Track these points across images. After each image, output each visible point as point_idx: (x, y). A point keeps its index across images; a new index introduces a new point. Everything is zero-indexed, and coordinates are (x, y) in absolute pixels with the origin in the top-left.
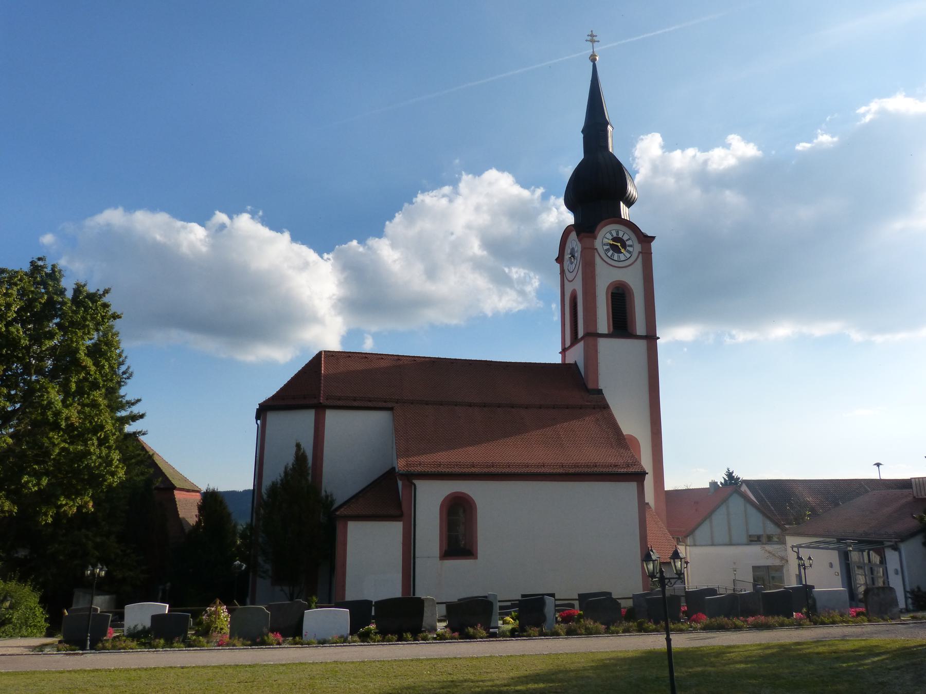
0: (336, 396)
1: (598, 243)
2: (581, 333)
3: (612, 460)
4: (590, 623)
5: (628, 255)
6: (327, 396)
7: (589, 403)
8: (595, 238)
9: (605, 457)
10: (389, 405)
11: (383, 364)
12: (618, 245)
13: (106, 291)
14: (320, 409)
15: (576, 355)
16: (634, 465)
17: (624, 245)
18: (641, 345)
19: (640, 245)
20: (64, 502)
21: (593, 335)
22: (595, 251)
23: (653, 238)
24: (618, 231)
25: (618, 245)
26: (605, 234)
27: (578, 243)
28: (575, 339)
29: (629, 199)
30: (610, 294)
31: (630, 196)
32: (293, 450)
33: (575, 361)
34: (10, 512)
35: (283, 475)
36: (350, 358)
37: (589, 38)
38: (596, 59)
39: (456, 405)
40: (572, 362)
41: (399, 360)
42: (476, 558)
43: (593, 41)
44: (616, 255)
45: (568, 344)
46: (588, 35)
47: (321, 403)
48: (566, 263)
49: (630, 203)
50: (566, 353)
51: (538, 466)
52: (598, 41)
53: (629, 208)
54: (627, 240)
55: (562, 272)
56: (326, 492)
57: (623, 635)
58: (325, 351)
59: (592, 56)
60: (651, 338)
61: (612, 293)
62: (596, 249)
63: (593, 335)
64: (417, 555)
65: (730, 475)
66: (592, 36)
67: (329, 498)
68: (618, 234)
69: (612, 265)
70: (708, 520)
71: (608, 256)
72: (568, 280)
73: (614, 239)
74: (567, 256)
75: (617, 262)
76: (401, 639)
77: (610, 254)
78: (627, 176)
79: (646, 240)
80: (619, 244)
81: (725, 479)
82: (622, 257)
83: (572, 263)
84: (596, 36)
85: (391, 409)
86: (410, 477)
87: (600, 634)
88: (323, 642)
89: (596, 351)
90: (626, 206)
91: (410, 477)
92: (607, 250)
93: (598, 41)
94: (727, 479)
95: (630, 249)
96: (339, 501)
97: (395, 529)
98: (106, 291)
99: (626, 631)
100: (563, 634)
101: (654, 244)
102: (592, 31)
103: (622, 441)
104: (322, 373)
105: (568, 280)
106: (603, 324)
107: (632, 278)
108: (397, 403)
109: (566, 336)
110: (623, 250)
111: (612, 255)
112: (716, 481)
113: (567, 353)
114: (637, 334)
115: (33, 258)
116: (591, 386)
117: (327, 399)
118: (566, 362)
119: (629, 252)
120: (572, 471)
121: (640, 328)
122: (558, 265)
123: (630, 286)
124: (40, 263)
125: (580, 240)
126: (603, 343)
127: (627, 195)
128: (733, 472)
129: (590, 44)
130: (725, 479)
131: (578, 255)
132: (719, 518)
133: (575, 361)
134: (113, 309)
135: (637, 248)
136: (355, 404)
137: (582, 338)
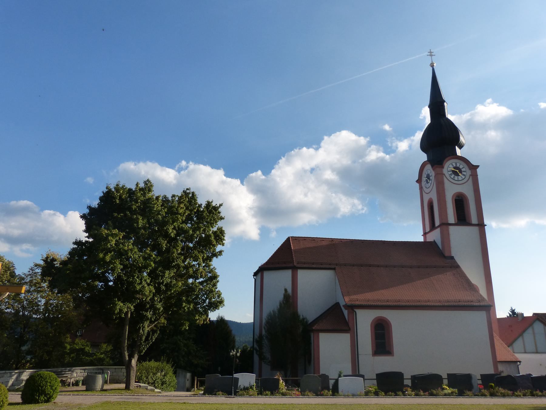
0: (302, 262)
1: (445, 171)
2: (437, 223)
3: (469, 298)
4: (502, 390)
5: (464, 177)
6: (298, 262)
7: (447, 265)
8: (443, 167)
9: (463, 296)
10: (333, 267)
11: (324, 243)
12: (456, 172)
13: (221, 205)
14: (294, 269)
15: (435, 236)
16: (483, 301)
17: (461, 171)
18: (476, 229)
19: (470, 171)
20: (197, 318)
21: (445, 224)
22: (444, 175)
23: (478, 166)
24: (456, 163)
25: (456, 172)
26: (449, 165)
27: (432, 171)
28: (433, 227)
29: (460, 144)
30: (454, 200)
31: (462, 142)
32: (283, 292)
33: (434, 240)
34: (164, 323)
35: (279, 307)
36: (305, 241)
37: (429, 54)
38: (434, 66)
39: (370, 266)
40: (432, 240)
41: (332, 241)
42: (393, 355)
43: (431, 55)
44: (456, 177)
45: (428, 229)
46: (428, 52)
47: (295, 266)
48: (424, 183)
49: (461, 147)
50: (427, 235)
51: (426, 301)
52: (434, 55)
53: (460, 149)
54: (462, 168)
55: (421, 188)
56: (303, 316)
57: (523, 397)
58: (291, 237)
59: (431, 64)
60: (481, 226)
61: (455, 200)
62: (444, 174)
63: (445, 224)
64: (359, 353)
65: (513, 311)
66: (430, 52)
67: (305, 320)
68: (456, 165)
69: (453, 183)
70: (521, 337)
71: (465, 178)
72: (426, 193)
73: (455, 168)
74: (424, 179)
75: (457, 181)
76: (396, 395)
77: (452, 176)
78: (459, 131)
79: (473, 168)
80: (458, 171)
81: (510, 314)
82: (460, 178)
83: (428, 183)
84: (433, 52)
85: (334, 269)
86: (352, 308)
87: (509, 396)
88: (348, 396)
89: (448, 234)
90: (459, 148)
91: (352, 308)
92: (451, 174)
93: (434, 55)
94: (511, 314)
95: (450, 173)
96: (310, 321)
97: (345, 338)
98: (221, 205)
99: (525, 395)
100: (488, 395)
101: (478, 170)
102: (430, 50)
103: (472, 288)
104: (292, 249)
105: (426, 193)
106: (451, 218)
107: (467, 190)
108: (337, 265)
109: (426, 226)
110: (460, 174)
111: (458, 178)
112: (522, 313)
113: (428, 236)
114: (473, 223)
115: (184, 189)
116: (447, 254)
117: (298, 264)
118: (427, 241)
119: (464, 175)
120: (446, 304)
121: (474, 220)
122: (418, 185)
123: (466, 195)
124: (188, 191)
125: (433, 170)
126: (451, 228)
127: (460, 142)
128: (515, 310)
129: (430, 57)
130: (510, 314)
131: (432, 178)
132: (528, 336)
133: (434, 240)
134: (222, 215)
135: (469, 172)
136: (314, 266)
137: (438, 227)
